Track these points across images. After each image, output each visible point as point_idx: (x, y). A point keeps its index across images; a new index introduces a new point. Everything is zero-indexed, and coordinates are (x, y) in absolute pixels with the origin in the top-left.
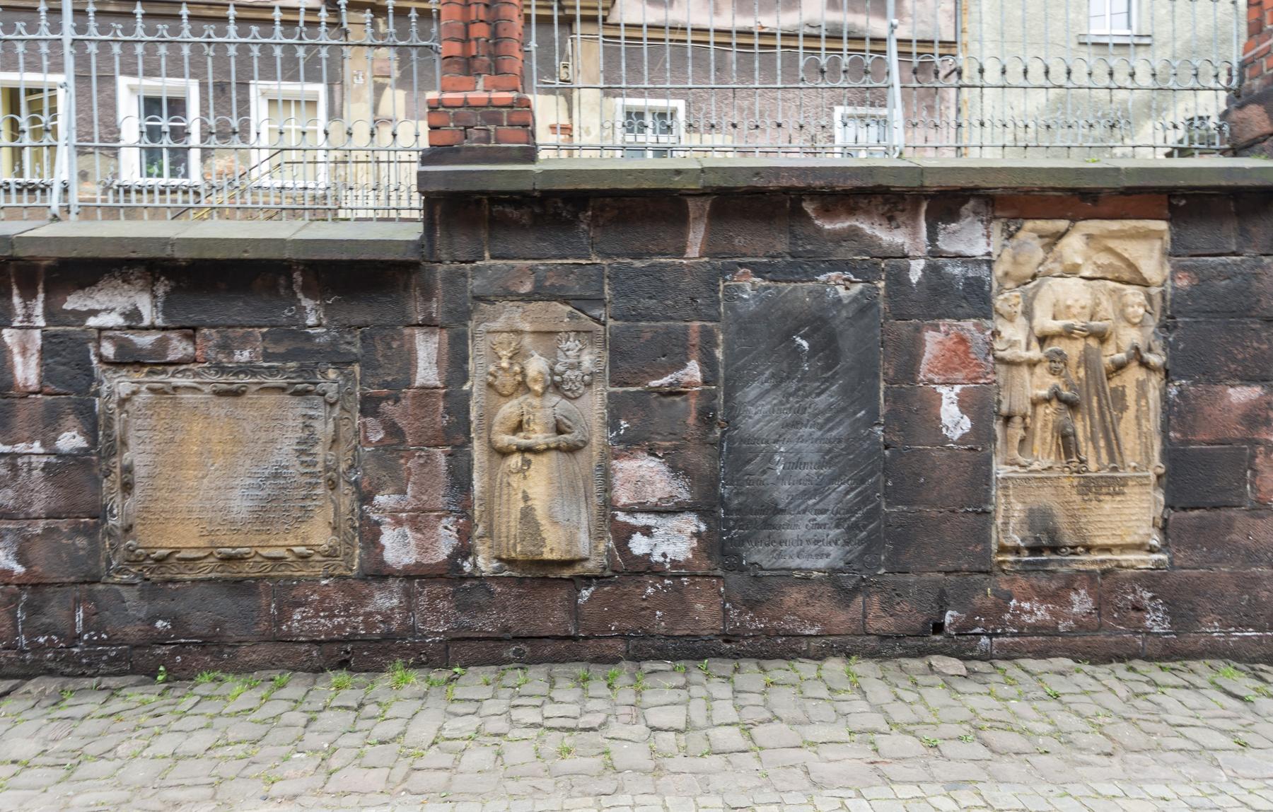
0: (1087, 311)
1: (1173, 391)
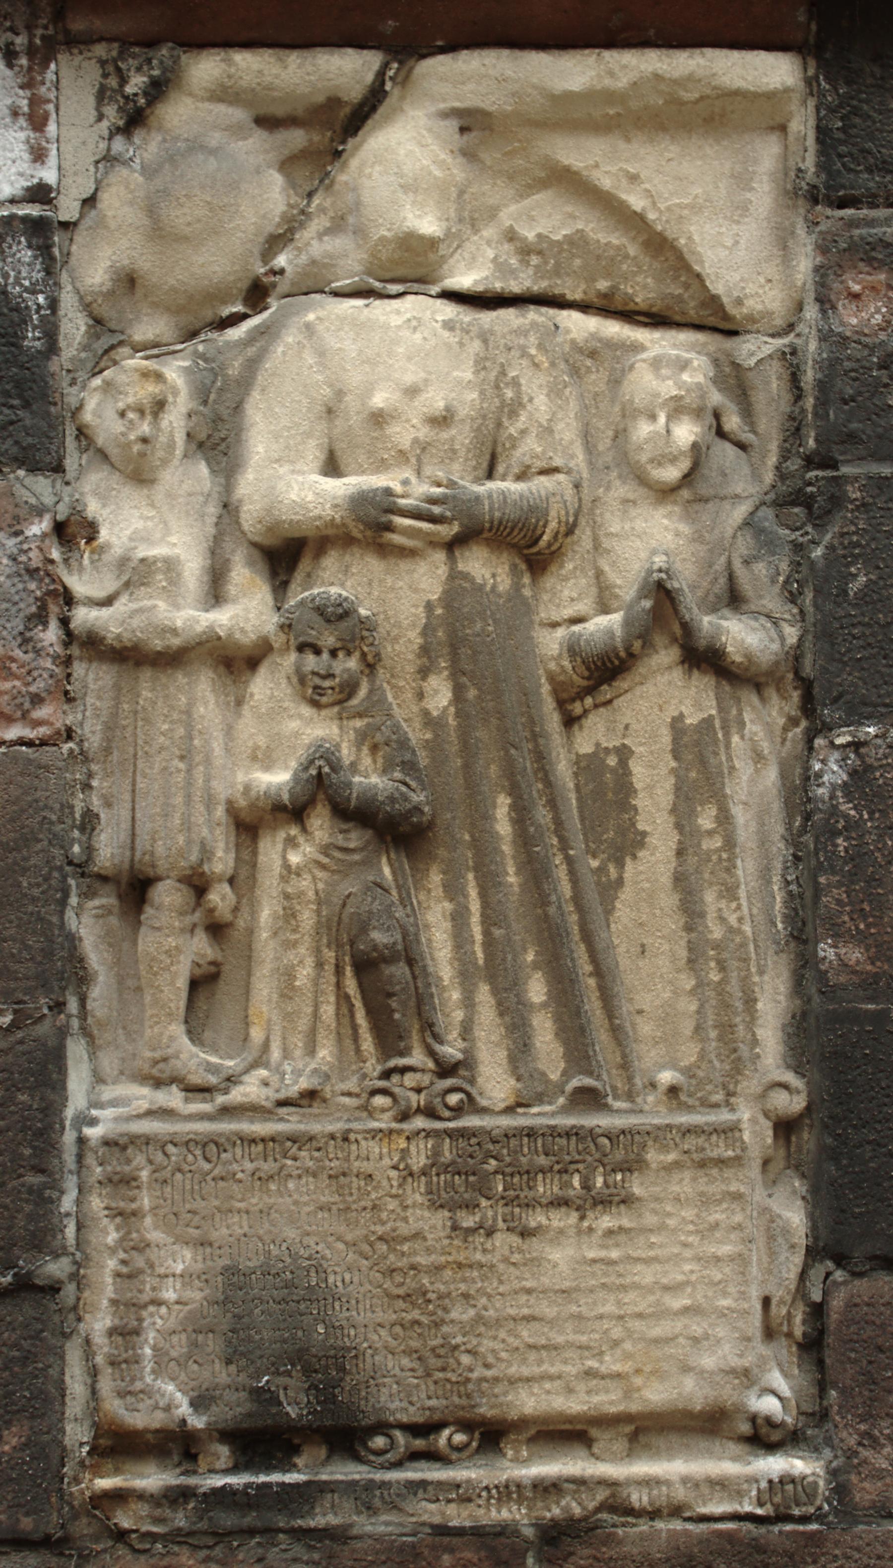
0: (461, 436)
1: (832, 771)
